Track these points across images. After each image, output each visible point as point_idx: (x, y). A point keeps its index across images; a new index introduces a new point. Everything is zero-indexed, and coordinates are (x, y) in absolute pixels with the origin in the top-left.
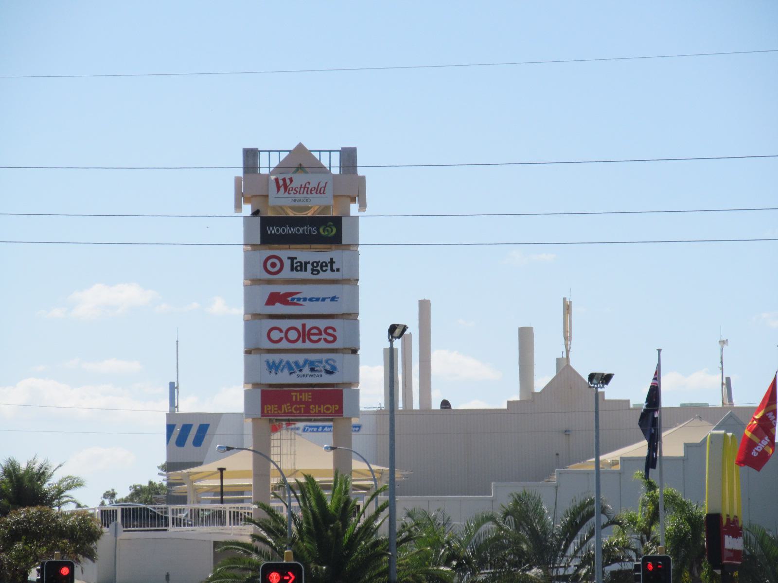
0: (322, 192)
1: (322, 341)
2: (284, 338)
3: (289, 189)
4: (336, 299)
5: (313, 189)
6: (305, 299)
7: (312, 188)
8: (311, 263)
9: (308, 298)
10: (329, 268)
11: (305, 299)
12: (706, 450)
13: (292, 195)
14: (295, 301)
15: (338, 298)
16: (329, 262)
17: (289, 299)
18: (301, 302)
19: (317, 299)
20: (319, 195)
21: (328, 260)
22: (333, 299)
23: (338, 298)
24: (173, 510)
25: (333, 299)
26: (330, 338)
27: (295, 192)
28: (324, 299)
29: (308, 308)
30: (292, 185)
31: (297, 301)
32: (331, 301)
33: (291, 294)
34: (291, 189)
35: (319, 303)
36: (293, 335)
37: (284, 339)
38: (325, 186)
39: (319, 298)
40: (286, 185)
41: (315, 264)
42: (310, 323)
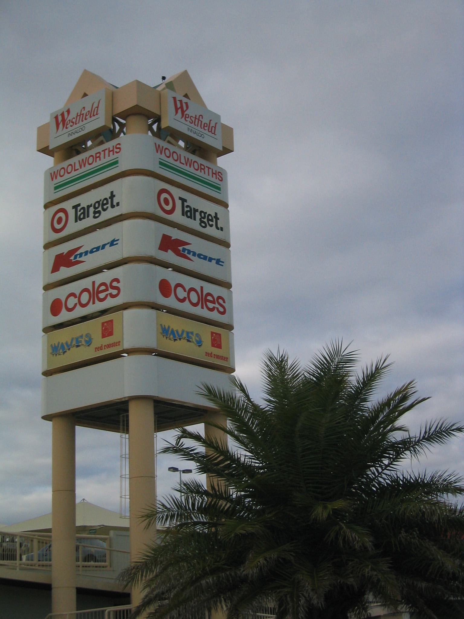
0: (95, 114)
1: (109, 297)
2: (187, 299)
3: (67, 122)
4: (115, 243)
5: (206, 125)
6: (86, 253)
7: (86, 113)
8: (199, 211)
9: (197, 253)
10: (109, 205)
11: (86, 253)
12: (154, 462)
13: (70, 128)
14: (186, 253)
15: (118, 240)
16: (110, 198)
17: (72, 258)
18: (190, 256)
19: (98, 249)
20: (93, 118)
21: (108, 195)
22: (112, 243)
23: (118, 240)
24: (25, 545)
25: (112, 243)
26: (115, 292)
27: (72, 124)
28: (103, 247)
29: (196, 265)
30: (70, 117)
31: (80, 257)
32: (110, 246)
33: (72, 252)
34: (69, 122)
35: (101, 251)
36: (194, 297)
37: (78, 305)
38: (98, 105)
39: (87, 251)
40: (65, 119)
41: (97, 205)
42: (98, 278)
